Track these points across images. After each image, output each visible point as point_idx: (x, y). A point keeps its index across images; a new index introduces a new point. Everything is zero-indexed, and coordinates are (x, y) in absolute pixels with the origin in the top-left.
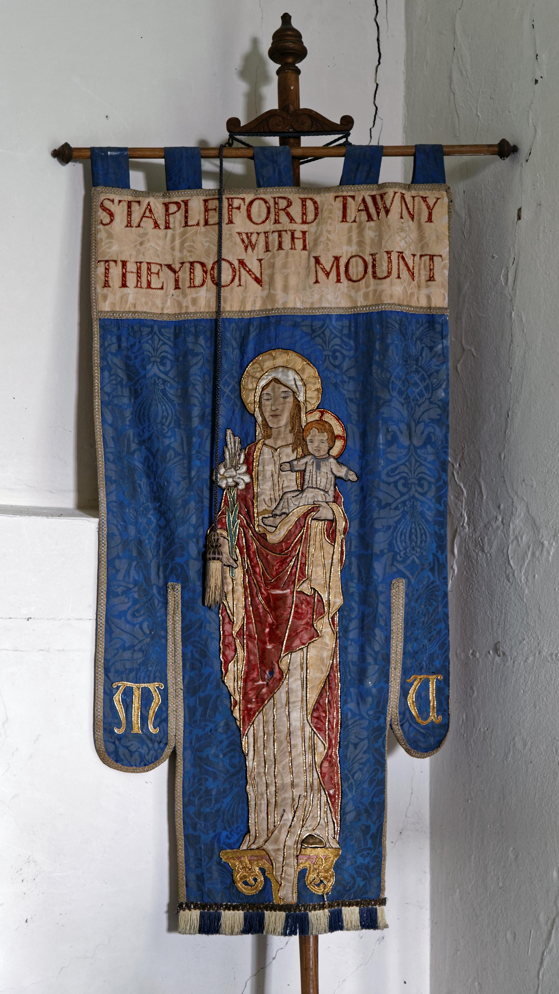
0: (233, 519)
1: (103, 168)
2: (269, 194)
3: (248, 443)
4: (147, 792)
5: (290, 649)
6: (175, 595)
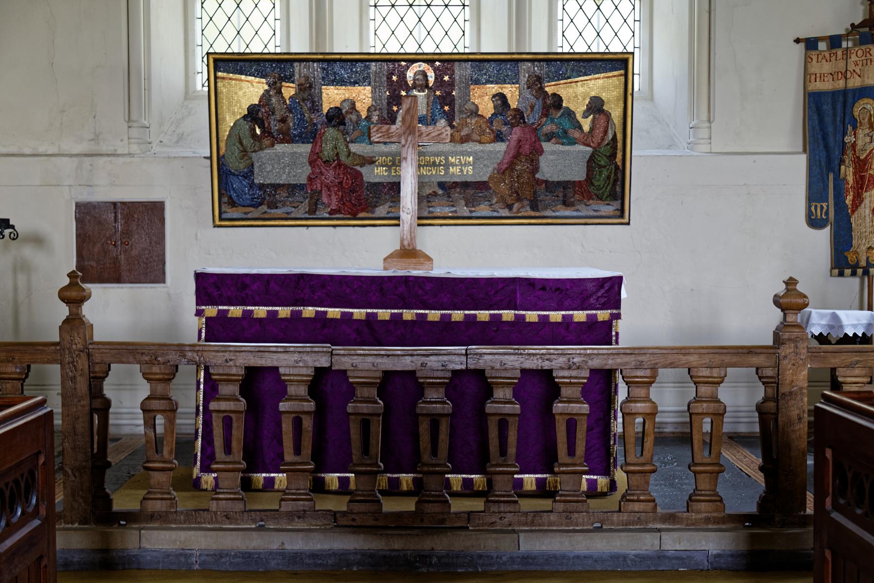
0: (850, 152)
1: (811, 44)
2: (863, 47)
3: (855, 128)
4: (824, 236)
5: (866, 191)
6: (831, 176)
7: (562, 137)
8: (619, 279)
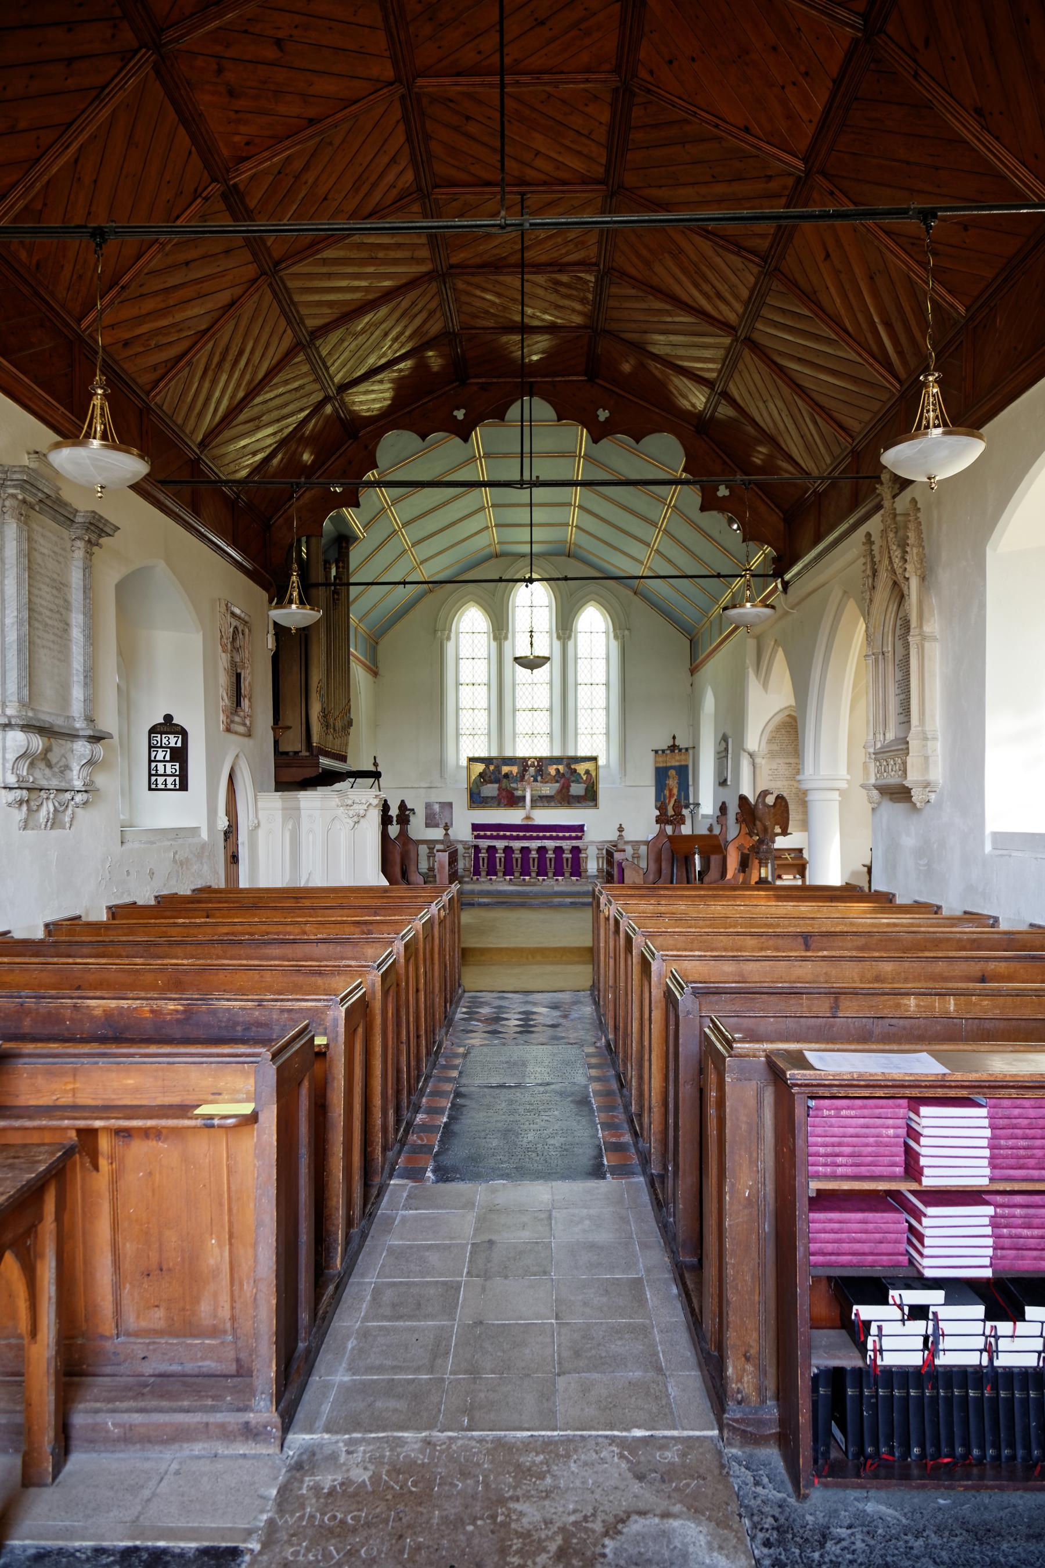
1: (656, 752)
7: (577, 781)
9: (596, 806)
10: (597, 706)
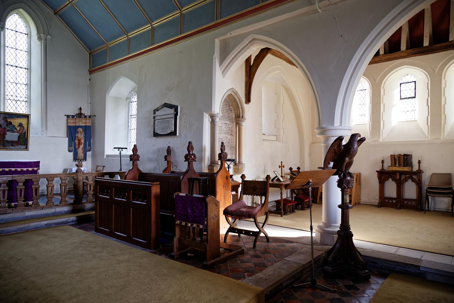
1: (68, 116)
4: (72, 154)
7: (12, 131)
8: (39, 162)
9: (27, 148)
10: (21, 82)
